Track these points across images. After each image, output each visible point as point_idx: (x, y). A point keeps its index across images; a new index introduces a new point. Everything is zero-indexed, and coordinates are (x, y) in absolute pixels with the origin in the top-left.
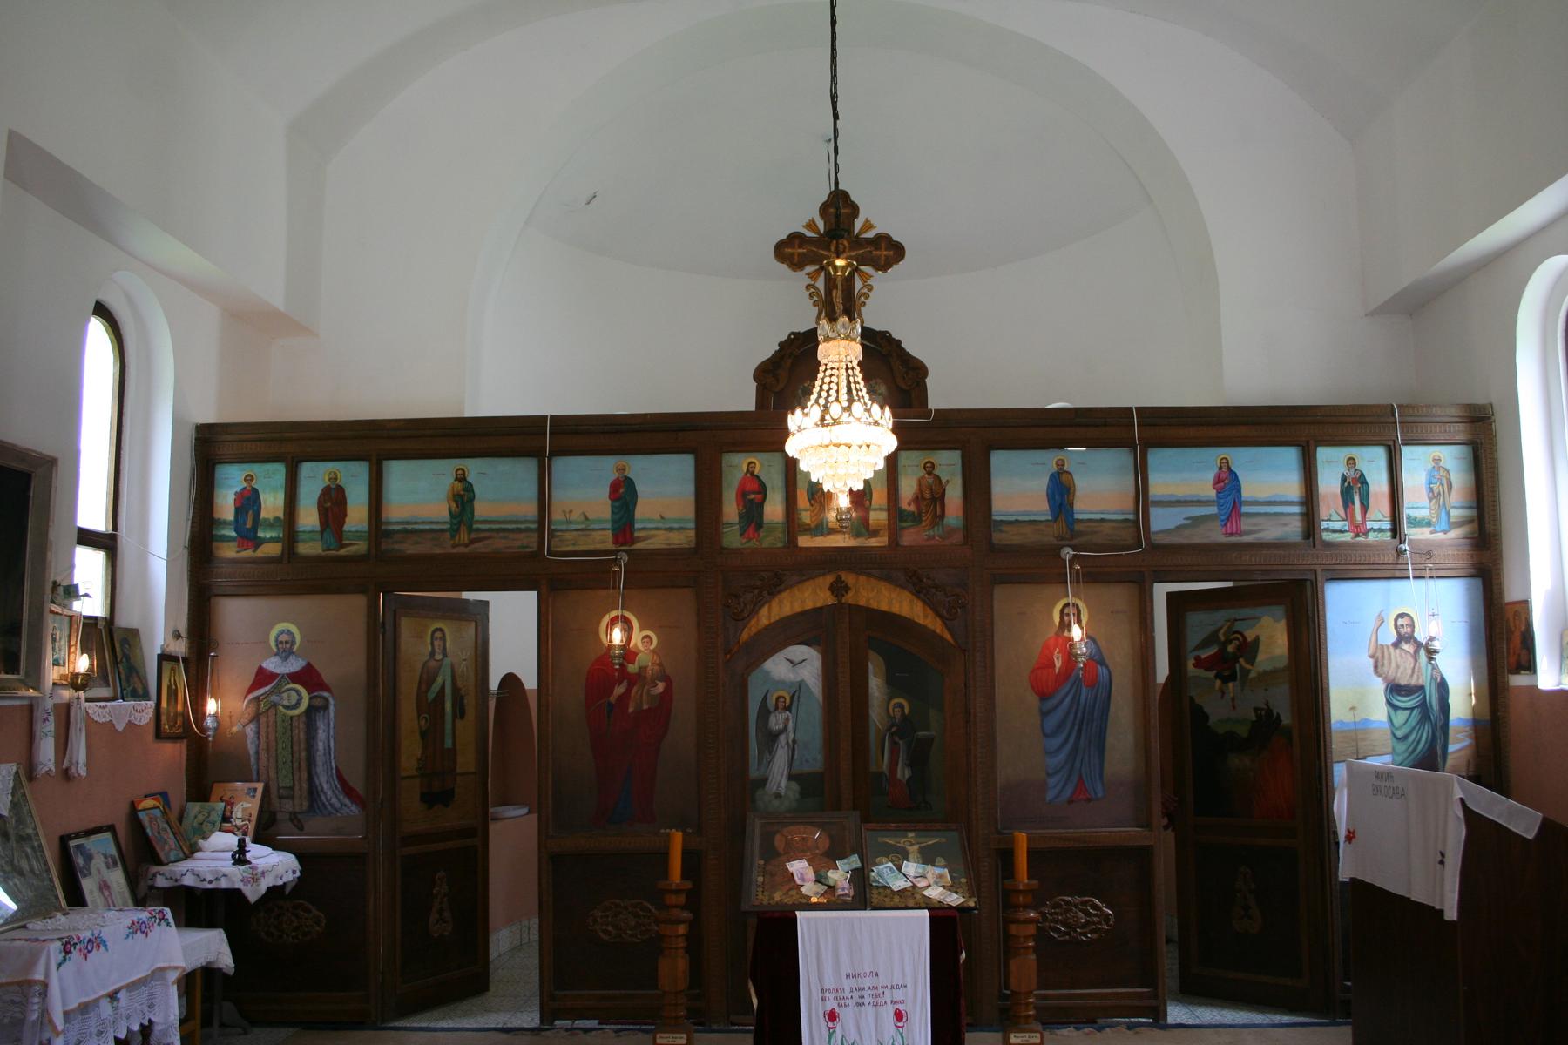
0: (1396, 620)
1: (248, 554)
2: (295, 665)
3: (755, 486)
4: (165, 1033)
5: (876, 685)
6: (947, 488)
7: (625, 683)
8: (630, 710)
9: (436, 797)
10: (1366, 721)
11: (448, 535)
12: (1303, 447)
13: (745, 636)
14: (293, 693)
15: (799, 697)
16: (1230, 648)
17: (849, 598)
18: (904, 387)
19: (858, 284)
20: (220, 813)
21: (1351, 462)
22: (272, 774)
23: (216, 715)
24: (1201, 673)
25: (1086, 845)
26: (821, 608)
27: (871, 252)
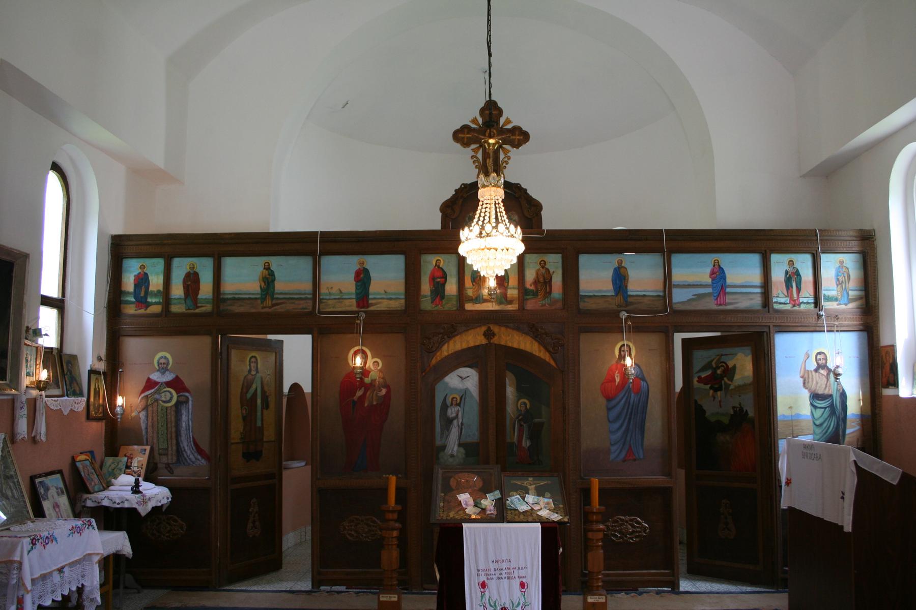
0: (816, 356)
1: (142, 311)
2: (169, 377)
3: (440, 274)
4: (91, 592)
5: (510, 391)
6: (553, 276)
7: (363, 389)
8: (366, 405)
9: (251, 455)
10: (798, 415)
11: (259, 301)
12: (763, 254)
13: (434, 362)
14: (168, 394)
15: (465, 398)
16: (719, 372)
17: (495, 340)
18: (529, 217)
19: (502, 156)
20: (125, 463)
21: (791, 263)
22: (155, 441)
23: (122, 406)
24: (702, 386)
25: (632, 486)
26: (478, 346)
27: (510, 137)
